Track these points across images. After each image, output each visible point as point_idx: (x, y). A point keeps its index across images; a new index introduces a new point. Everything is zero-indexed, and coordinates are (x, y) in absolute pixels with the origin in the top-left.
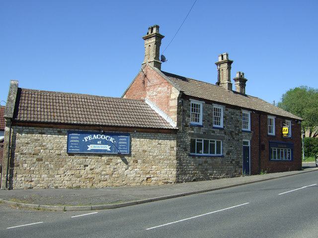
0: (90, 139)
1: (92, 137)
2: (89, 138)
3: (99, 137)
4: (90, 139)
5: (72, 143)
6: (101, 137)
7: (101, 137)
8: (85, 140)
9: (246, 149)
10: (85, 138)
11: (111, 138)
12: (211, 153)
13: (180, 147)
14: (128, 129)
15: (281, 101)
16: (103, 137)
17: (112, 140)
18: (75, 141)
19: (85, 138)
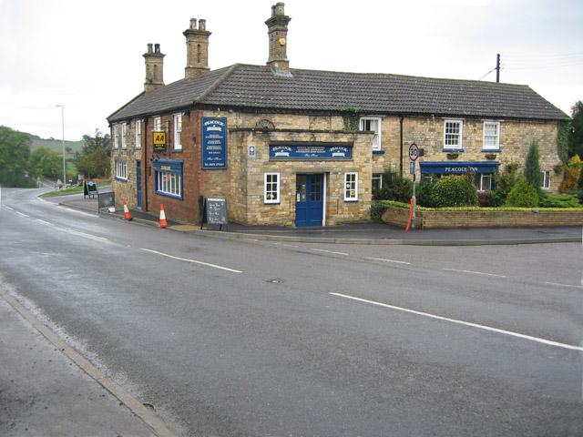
5: (210, 151)
17: (290, 149)
18: (215, 148)
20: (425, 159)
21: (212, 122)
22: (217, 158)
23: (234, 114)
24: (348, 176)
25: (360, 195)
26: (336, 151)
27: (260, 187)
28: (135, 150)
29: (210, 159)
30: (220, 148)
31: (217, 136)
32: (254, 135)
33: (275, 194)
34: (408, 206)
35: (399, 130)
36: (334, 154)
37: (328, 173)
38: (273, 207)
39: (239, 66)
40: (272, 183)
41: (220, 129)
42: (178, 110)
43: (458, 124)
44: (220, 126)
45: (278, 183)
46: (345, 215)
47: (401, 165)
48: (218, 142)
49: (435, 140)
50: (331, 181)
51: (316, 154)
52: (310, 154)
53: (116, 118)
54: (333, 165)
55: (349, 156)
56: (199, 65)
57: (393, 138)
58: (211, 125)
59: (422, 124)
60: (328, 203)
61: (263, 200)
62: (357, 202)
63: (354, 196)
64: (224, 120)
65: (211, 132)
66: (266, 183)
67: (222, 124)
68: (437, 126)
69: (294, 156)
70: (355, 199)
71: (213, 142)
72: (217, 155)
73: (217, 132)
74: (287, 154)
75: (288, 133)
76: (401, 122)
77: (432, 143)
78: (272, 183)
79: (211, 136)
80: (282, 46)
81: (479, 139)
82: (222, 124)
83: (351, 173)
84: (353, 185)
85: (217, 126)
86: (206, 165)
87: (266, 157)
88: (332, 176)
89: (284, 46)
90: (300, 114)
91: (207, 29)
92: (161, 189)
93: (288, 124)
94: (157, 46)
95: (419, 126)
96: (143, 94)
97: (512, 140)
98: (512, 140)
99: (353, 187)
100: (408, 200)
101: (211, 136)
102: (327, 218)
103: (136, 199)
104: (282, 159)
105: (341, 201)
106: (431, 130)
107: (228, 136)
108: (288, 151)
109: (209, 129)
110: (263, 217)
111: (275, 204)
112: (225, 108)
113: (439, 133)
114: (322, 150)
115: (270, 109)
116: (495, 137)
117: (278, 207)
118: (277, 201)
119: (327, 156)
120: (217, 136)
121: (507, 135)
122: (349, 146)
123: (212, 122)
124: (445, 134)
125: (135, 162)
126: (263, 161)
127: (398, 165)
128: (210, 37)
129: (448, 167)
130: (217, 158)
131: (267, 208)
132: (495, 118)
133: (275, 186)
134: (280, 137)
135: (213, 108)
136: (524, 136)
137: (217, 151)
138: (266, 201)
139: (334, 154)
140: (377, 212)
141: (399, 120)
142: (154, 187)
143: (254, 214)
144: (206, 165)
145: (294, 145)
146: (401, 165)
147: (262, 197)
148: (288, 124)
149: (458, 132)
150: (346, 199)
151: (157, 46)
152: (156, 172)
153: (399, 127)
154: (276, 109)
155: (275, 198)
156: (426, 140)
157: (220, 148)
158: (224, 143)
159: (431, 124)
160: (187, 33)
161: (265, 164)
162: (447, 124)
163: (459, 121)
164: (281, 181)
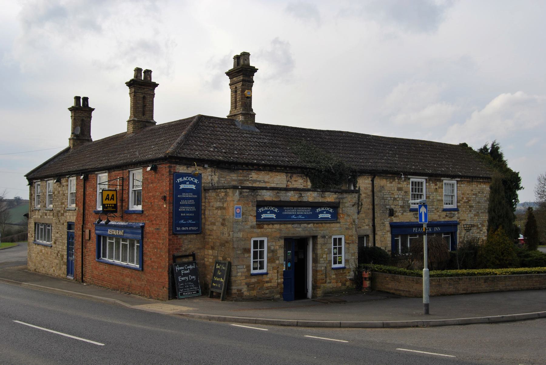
0: (262, 210)
1: (183, 179)
2: (181, 180)
3: (187, 179)
4: (181, 181)
5: (183, 212)
6: (189, 179)
7: (189, 179)
8: (178, 182)
9: (70, 226)
10: (178, 180)
11: (196, 180)
12: (334, 248)
13: (478, 155)
14: (38, 170)
15: (469, 146)
16: (190, 179)
17: (276, 210)
18: (188, 209)
19: (178, 180)
20: (395, 220)
21: (185, 179)
22: (190, 221)
23: (209, 170)
24: (335, 240)
25: (347, 261)
26: (322, 212)
27: (246, 255)
28: (65, 211)
29: (182, 222)
30: (193, 209)
31: (190, 195)
32: (241, 193)
33: (262, 263)
34: (98, 232)
35: (370, 189)
36: (320, 216)
37: (315, 238)
38: (260, 278)
39: (201, 118)
40: (259, 250)
41: (193, 187)
42: (142, 164)
43: (422, 183)
44: (194, 184)
45: (265, 250)
46: (332, 284)
47: (374, 226)
48: (192, 202)
49: (403, 199)
50: (319, 246)
51: (303, 215)
52: (297, 215)
53: (36, 175)
54: (320, 230)
55: (335, 217)
56: (144, 118)
57: (366, 197)
58: (184, 183)
59: (391, 183)
60: (315, 271)
61: (250, 270)
62: (344, 268)
63: (340, 263)
64: (199, 177)
65: (185, 190)
66: (252, 250)
67: (196, 181)
68: (404, 185)
69: (282, 219)
70: (342, 265)
71: (184, 202)
72: (190, 218)
73: (190, 190)
74: (274, 216)
75: (370, 193)
76: (373, 181)
77: (401, 203)
78: (259, 250)
79: (184, 195)
80: (248, 97)
81: (439, 198)
82: (196, 181)
83: (338, 237)
84: (340, 249)
85: (191, 183)
86: (178, 229)
87: (252, 221)
88: (320, 241)
89: (250, 98)
90: (271, 170)
91: (153, 80)
92: (104, 256)
93: (265, 182)
94: (86, 99)
95: (389, 185)
96: (67, 150)
97: (467, 198)
98: (467, 198)
99: (340, 253)
100: (336, 257)
101: (184, 195)
102: (315, 288)
103: (65, 267)
104: (269, 221)
105: (329, 268)
106: (400, 189)
107: (203, 195)
108: (275, 213)
109: (182, 186)
110: (248, 290)
111: (262, 274)
112: (201, 162)
113: (406, 192)
114: (307, 211)
115: (247, 164)
116: (452, 196)
117: (266, 279)
118: (264, 271)
119: (313, 218)
120: (190, 195)
121: (463, 194)
122: (335, 206)
123: (185, 179)
124: (411, 193)
125: (66, 224)
126: (250, 224)
127: (371, 225)
128: (156, 89)
129: (415, 227)
130: (190, 221)
131: (253, 280)
132: (452, 177)
133: (262, 253)
134: (268, 196)
135: (188, 162)
136: (475, 194)
137: (190, 212)
138: (253, 272)
139: (320, 216)
140: (358, 280)
141: (370, 179)
142: (95, 254)
143: (240, 287)
144: (178, 229)
145: (281, 205)
146: (374, 226)
147: (248, 267)
148: (265, 182)
149: (422, 191)
150: (334, 266)
151: (86, 99)
152: (99, 237)
153: (370, 186)
154: (253, 165)
155: (262, 268)
156: (395, 199)
157: (193, 209)
158: (198, 203)
159: (399, 183)
160: (130, 84)
161: (252, 227)
162: (412, 182)
163: (422, 180)
164: (269, 248)
